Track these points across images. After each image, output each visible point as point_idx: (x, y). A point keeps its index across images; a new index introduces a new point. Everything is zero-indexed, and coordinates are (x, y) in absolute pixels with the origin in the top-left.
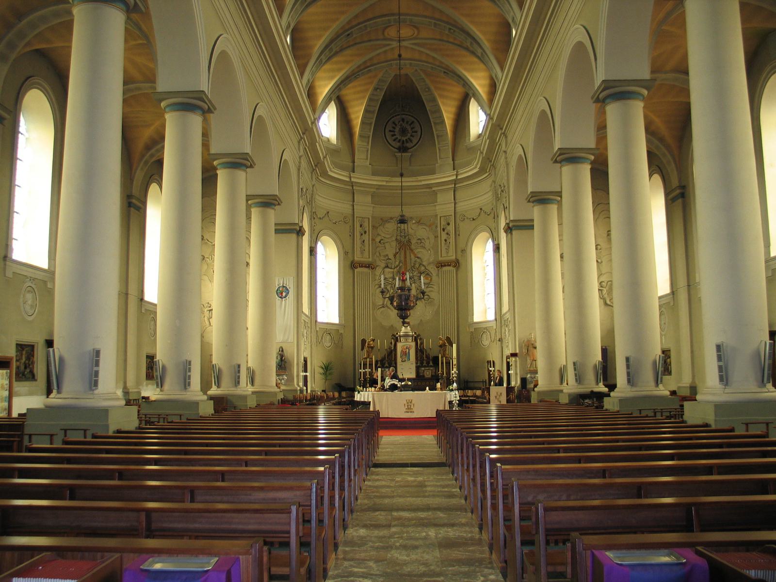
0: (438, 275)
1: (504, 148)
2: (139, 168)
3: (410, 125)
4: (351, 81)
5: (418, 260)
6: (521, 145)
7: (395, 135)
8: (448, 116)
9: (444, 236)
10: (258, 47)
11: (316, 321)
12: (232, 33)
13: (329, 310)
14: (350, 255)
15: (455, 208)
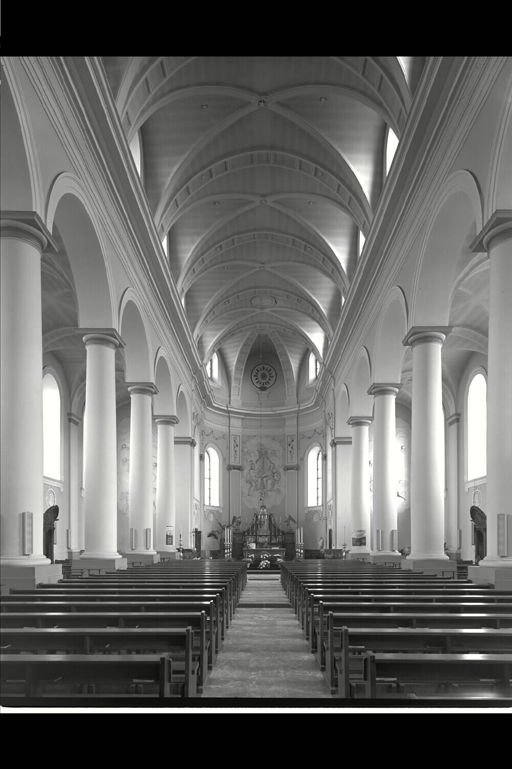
0: (285, 475)
1: (332, 387)
2: (76, 394)
3: (269, 371)
4: (228, 339)
5: (272, 465)
6: (365, 347)
7: (258, 379)
8: (294, 365)
9: (290, 448)
10: (119, 211)
11: (204, 505)
12: (137, 288)
13: (214, 498)
14: (227, 461)
15: (298, 429)
